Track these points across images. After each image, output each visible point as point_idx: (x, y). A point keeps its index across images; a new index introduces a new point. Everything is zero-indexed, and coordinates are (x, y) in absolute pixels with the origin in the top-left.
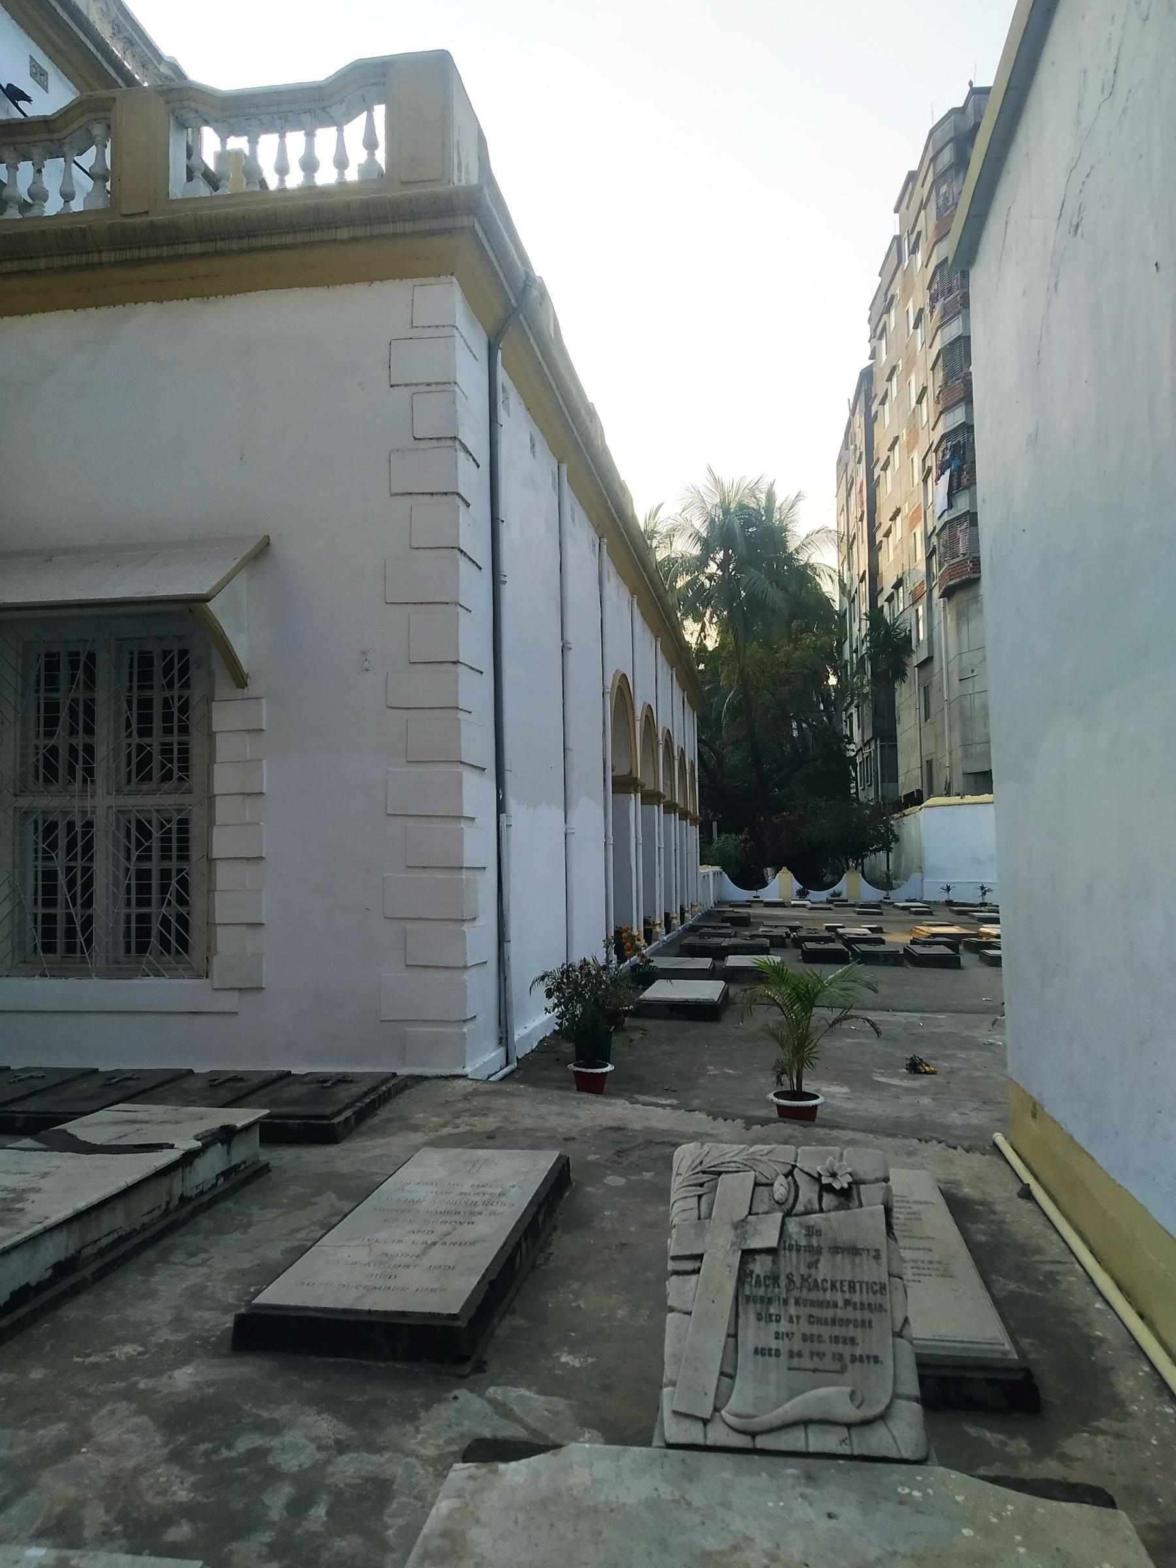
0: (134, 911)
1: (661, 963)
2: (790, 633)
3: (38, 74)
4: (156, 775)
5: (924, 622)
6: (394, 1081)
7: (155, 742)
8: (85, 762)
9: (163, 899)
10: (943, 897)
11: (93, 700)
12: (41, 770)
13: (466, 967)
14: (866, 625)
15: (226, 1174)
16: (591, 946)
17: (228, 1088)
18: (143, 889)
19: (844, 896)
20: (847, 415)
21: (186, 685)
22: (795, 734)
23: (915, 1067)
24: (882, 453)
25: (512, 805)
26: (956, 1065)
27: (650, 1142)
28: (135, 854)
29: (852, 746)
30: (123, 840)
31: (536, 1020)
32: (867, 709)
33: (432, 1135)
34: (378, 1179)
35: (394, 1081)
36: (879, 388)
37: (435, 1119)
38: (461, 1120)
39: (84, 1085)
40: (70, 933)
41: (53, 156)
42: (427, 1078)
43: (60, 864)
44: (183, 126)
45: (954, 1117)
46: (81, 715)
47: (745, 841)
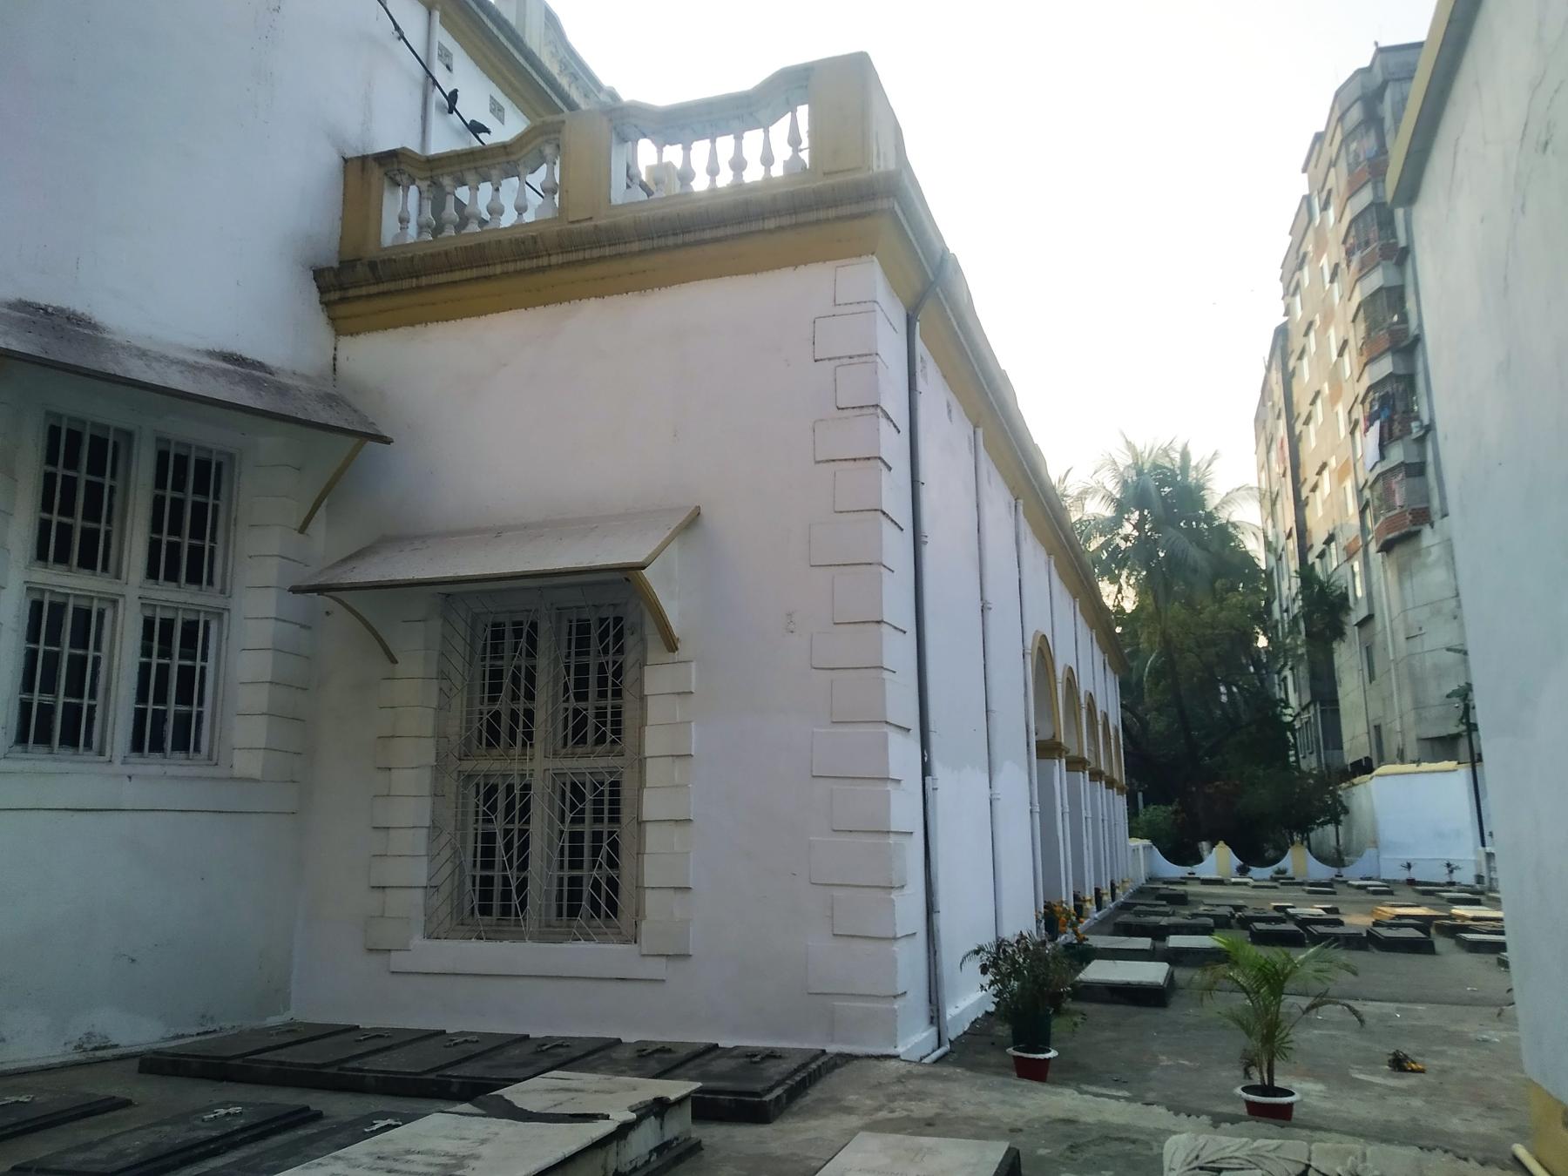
0: (567, 873)
1: (1098, 941)
2: (1214, 591)
3: (497, 110)
4: (591, 738)
5: (1358, 579)
6: (824, 1059)
7: (590, 707)
8: (526, 726)
9: (594, 862)
10: (1404, 875)
11: (534, 667)
12: (485, 734)
13: (895, 939)
14: (1296, 583)
15: (660, 1150)
16: (1021, 920)
17: (657, 1059)
18: (576, 851)
19: (1290, 873)
20: (1263, 372)
21: (620, 651)
22: (1224, 699)
23: (1399, 1064)
24: (1303, 408)
25: (937, 767)
26: (1448, 1063)
27: (1107, 1138)
28: (569, 816)
29: (1289, 711)
30: (558, 802)
31: (970, 998)
32: (1303, 670)
33: (866, 1119)
34: (815, 1164)
35: (824, 1059)
36: (1296, 343)
37: (868, 1102)
38: (896, 1104)
39: (515, 1052)
40: (506, 895)
41: (508, 175)
42: (857, 1057)
43: (498, 826)
44: (623, 140)
45: (1455, 1124)
46: (523, 682)
47: (1176, 812)
